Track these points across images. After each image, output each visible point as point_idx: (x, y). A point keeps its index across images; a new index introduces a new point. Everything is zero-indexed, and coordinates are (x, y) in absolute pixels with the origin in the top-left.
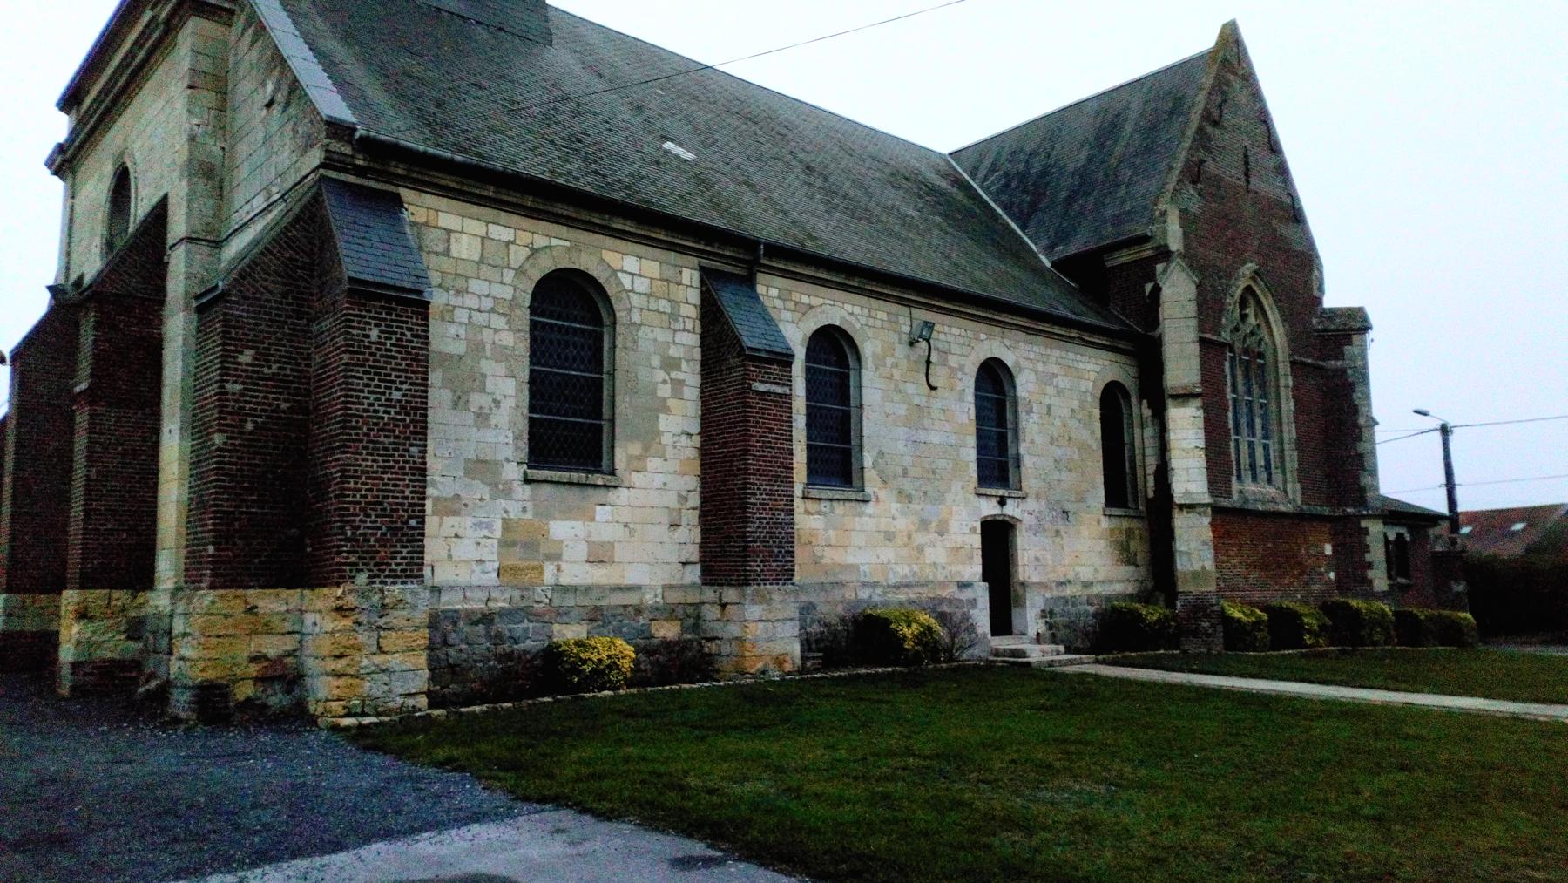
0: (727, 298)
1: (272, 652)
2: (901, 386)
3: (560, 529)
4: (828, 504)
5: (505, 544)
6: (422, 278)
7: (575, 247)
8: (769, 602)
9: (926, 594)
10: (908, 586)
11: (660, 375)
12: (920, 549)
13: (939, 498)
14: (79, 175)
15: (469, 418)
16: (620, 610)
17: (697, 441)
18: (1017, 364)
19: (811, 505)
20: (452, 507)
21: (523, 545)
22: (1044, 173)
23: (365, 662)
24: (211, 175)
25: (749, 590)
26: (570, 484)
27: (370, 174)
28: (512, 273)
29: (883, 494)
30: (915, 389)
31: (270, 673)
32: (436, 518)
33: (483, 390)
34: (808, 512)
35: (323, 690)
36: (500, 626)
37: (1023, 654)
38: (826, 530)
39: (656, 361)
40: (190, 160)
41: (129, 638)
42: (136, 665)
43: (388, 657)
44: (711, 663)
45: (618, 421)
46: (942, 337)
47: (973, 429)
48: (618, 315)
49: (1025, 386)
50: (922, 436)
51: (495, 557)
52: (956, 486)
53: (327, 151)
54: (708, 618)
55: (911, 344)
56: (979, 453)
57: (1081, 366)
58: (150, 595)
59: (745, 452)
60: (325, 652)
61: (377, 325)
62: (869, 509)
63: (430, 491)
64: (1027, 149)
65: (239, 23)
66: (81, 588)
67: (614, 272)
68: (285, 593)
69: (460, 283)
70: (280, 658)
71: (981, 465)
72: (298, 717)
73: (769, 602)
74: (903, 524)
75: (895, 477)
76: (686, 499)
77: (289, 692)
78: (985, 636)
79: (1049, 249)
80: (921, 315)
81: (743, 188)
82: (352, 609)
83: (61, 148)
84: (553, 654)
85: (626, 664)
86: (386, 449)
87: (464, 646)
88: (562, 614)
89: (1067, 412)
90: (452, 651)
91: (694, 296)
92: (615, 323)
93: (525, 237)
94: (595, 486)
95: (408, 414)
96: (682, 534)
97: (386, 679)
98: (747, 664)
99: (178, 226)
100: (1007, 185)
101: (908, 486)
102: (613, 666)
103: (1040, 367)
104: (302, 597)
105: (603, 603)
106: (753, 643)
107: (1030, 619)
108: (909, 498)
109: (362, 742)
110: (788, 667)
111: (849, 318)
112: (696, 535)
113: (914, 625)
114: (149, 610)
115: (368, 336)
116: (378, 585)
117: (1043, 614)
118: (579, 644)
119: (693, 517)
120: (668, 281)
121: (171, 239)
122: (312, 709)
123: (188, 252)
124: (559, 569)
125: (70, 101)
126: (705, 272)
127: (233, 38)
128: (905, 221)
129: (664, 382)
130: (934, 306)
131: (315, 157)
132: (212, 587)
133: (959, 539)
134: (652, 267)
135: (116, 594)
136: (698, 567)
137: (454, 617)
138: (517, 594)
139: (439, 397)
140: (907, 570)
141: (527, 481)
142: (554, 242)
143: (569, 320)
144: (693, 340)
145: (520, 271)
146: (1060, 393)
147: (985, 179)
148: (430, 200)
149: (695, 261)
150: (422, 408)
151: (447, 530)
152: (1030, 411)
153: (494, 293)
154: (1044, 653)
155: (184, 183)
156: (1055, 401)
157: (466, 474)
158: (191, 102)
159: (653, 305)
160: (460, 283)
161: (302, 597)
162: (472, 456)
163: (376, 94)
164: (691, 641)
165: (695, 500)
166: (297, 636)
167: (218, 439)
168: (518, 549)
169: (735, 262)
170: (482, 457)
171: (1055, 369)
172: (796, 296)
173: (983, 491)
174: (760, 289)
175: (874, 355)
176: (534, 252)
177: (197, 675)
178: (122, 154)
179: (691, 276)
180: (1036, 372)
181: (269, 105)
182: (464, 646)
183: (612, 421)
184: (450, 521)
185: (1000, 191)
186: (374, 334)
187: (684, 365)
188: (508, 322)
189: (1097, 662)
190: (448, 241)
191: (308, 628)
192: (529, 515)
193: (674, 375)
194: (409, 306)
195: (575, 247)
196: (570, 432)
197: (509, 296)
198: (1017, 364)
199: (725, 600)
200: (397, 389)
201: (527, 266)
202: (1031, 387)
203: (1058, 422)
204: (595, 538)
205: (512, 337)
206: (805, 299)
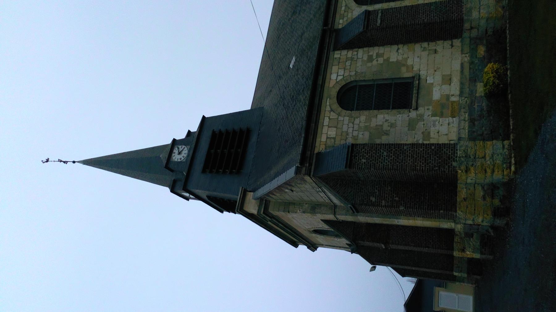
1: (482, 193)
3: (436, 95)
5: (442, 115)
11: (375, 62)
17: (400, 46)
20: (427, 135)
21: (443, 108)
24: (314, 208)
25: (465, 18)
26: (418, 93)
27: (311, 162)
28: (340, 117)
32: (431, 140)
33: (382, 126)
39: (369, 64)
40: (310, 213)
41: (472, 237)
43: (487, 154)
45: (393, 77)
51: (447, 119)
58: (456, 230)
61: (361, 160)
63: (420, 142)
67: (337, 82)
68: (459, 189)
72: (509, 186)
76: (425, 48)
77: (498, 188)
85: (496, 66)
88: (472, 93)
90: (485, 133)
91: (344, 52)
93: (327, 114)
95: (392, 150)
96: (439, 48)
99: (331, 217)
102: (497, 71)
104: (461, 183)
105: (468, 77)
112: (440, 42)
118: (485, 86)
120: (339, 62)
123: (339, 215)
124: (453, 95)
126: (335, 49)
129: (377, 61)
131: (307, 178)
132: (456, 211)
134: (335, 69)
135: (456, 240)
137: (471, 132)
139: (384, 140)
141: (417, 109)
142: (328, 104)
143: (353, 97)
144: (361, 51)
145: (339, 115)
150: (390, 145)
158: (293, 212)
159: (348, 67)
160: (344, 134)
165: (425, 44)
166: (476, 185)
167: (402, 208)
169: (330, 39)
172: (342, 12)
174: (340, 27)
176: (332, 110)
177: (489, 217)
178: (309, 231)
179: (337, 54)
181: (292, 191)
182: (484, 128)
183: (392, 79)
184: (432, 135)
186: (364, 161)
187: (370, 54)
192: (431, 107)
193: (374, 57)
194: (353, 151)
196: (399, 93)
197: (348, 118)
199: (469, 28)
200: (383, 153)
205: (362, 117)
206: (343, 8)
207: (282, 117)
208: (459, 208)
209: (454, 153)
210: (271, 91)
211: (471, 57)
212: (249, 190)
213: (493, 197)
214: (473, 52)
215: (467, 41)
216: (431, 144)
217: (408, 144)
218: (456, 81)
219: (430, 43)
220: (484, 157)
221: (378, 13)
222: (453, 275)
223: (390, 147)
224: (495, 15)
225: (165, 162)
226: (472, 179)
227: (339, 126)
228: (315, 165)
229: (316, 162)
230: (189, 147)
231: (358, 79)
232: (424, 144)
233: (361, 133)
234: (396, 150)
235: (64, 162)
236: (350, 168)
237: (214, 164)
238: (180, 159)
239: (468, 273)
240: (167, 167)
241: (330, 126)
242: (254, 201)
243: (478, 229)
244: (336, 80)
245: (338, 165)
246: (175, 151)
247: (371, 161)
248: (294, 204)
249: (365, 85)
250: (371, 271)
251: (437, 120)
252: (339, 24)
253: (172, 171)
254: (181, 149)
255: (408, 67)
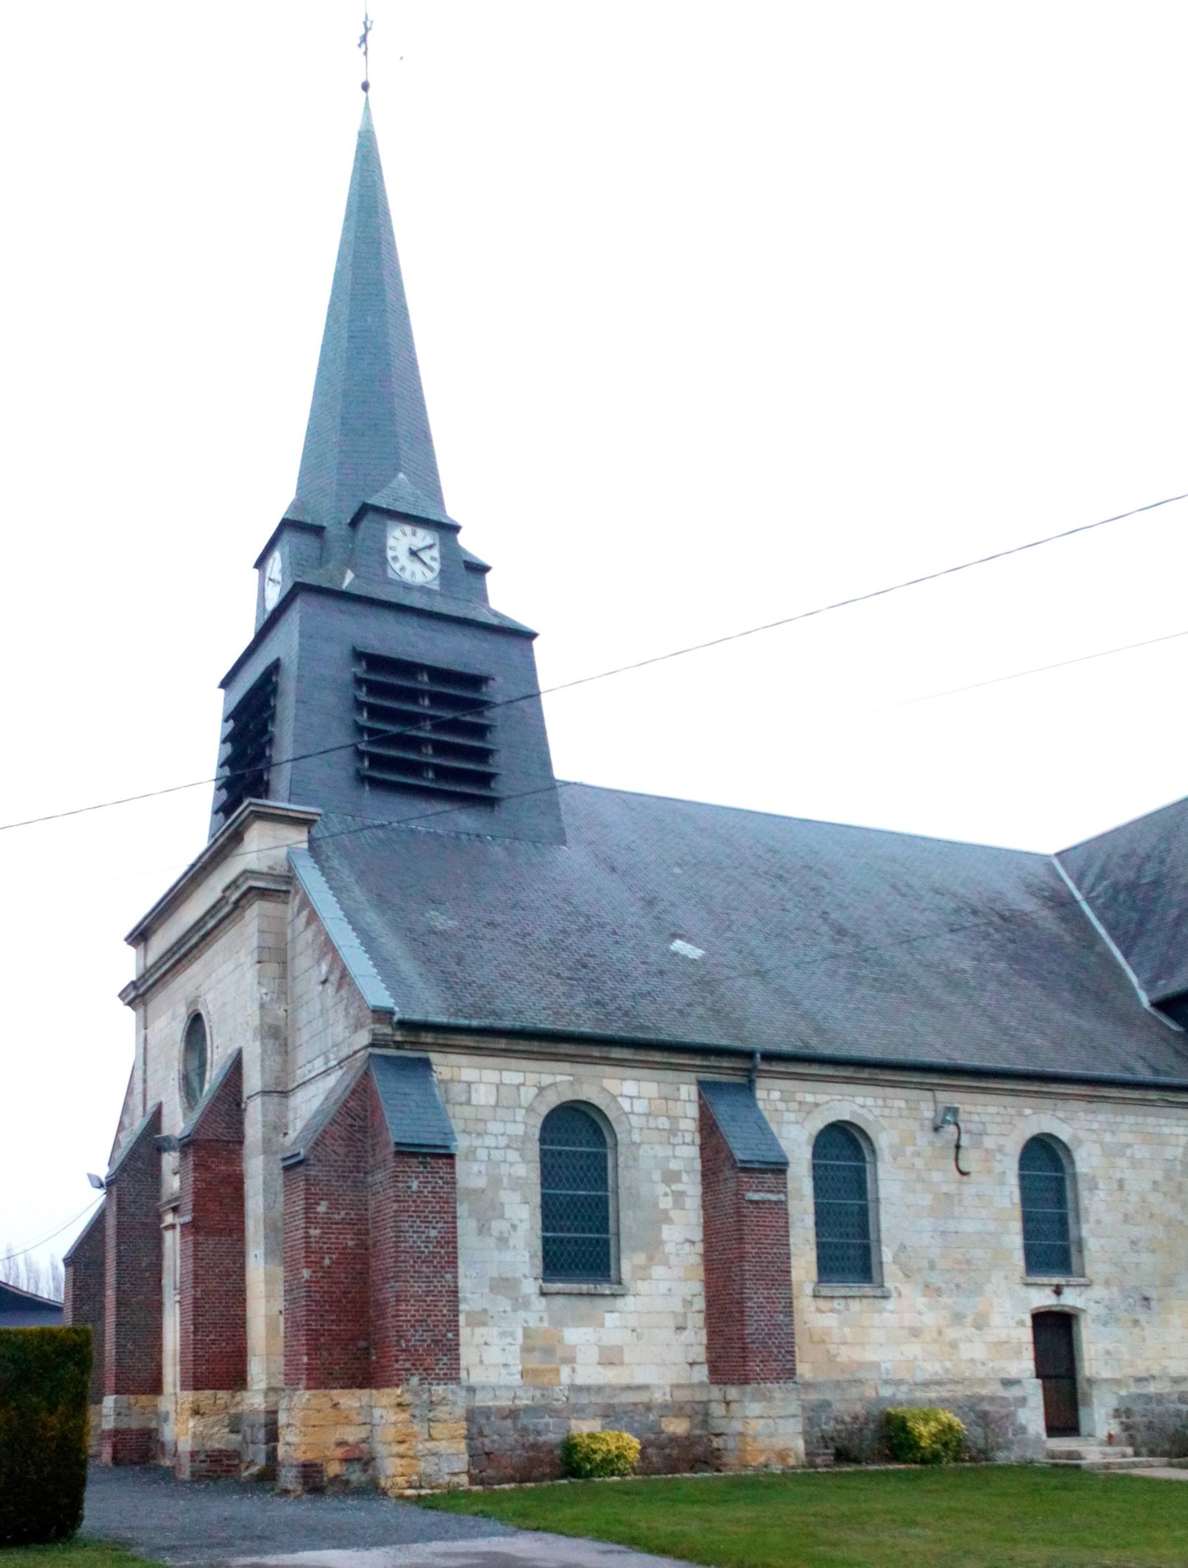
0: (721, 1110)
1: (351, 1439)
2: (925, 1175)
3: (573, 1335)
4: (842, 1301)
5: (527, 1350)
6: (449, 1134)
7: (577, 1081)
8: (770, 1399)
9: (960, 1391)
10: (939, 1383)
11: (661, 1188)
12: (954, 1345)
13: (977, 1289)
14: (151, 1008)
15: (492, 1242)
16: (631, 1408)
17: (700, 1248)
18: (1075, 1137)
19: (822, 1304)
20: (481, 1319)
21: (542, 1351)
22: (1156, 883)
23: (420, 1447)
24: (278, 1036)
25: (748, 1388)
26: (581, 1294)
27: (408, 1044)
28: (523, 1111)
29: (906, 1290)
30: (943, 1177)
31: (351, 1456)
32: (469, 1330)
33: (502, 1216)
34: (819, 1311)
35: (391, 1469)
36: (525, 1420)
37: (1078, 1456)
38: (840, 1328)
39: (657, 1176)
40: (261, 1025)
41: (232, 1432)
42: (237, 1454)
43: (437, 1443)
44: (719, 1458)
45: (622, 1237)
46: (976, 1118)
47: (1017, 1213)
48: (619, 1137)
49: (1086, 1160)
50: (952, 1225)
51: (518, 1361)
52: (997, 1277)
53: (374, 1034)
54: (715, 1415)
55: (936, 1129)
56: (1025, 1238)
57: (1166, 1130)
58: (245, 1394)
59: (742, 1258)
60: (390, 1439)
61: (417, 1178)
62: (890, 1305)
63: (462, 1307)
64: (1141, 852)
65: (295, 903)
66: (196, 1389)
67: (614, 1098)
69: (480, 1127)
70: (357, 1445)
71: (1029, 1252)
72: (372, 1490)
73: (770, 1399)
74: (930, 1319)
75: (920, 1270)
76: (691, 1303)
77: (365, 1471)
78: (1038, 1437)
79: (1149, 985)
80: (946, 1098)
81: (754, 981)
82: (408, 1405)
83: (134, 985)
84: (569, 1446)
85: (633, 1455)
86: (427, 1277)
87: (496, 1437)
88: (579, 1411)
89: (1147, 1186)
90: (486, 1441)
91: (693, 1111)
92: (616, 1145)
93: (532, 1078)
94: (603, 1295)
95: (442, 1247)
96: (688, 1336)
97: (437, 1461)
98: (749, 1458)
99: (253, 1080)
100: (1114, 898)
101: (936, 1279)
103: (1108, 1138)
104: (371, 1396)
105: (615, 1401)
106: (755, 1439)
107: (1099, 1417)
108: (939, 1292)
109: (421, 1504)
110: (792, 1461)
111: (861, 1111)
112: (703, 1337)
113: (933, 1424)
114: (244, 1407)
115: (409, 1187)
116: (426, 1386)
117: (1117, 1413)
118: (592, 1436)
119: (699, 1320)
120: (666, 1099)
121: (246, 1092)
122: (383, 1483)
123: (263, 1104)
124: (573, 1370)
125: (140, 936)
126: (702, 1084)
127: (289, 917)
128: (952, 980)
129: (666, 1195)
130: (953, 1086)
131: (364, 1038)
132: (308, 1388)
133: (1003, 1334)
135: (221, 1394)
136: (706, 1367)
137: (487, 1412)
138: (538, 1393)
139: (466, 1226)
140: (937, 1367)
141: (543, 1294)
142: (559, 1078)
143: (576, 1145)
144: (694, 1152)
145: (530, 1109)
146: (1135, 1164)
147: (1092, 890)
148: (453, 1059)
149: (692, 1076)
151: (478, 1340)
152: (1094, 1188)
153: (508, 1132)
154: (1105, 1455)
155: (258, 1044)
156: (1128, 1174)
157: (492, 1289)
158: (261, 975)
159: (652, 1124)
160: (480, 1127)
161: (371, 1396)
162: (495, 1275)
163: (408, 968)
164: (700, 1437)
165: (700, 1304)
166: (368, 1427)
167: (306, 1273)
168: (537, 1354)
169: (730, 1070)
170: (504, 1276)
171: (1129, 1138)
173: (1031, 1280)
174: (760, 1094)
175: (891, 1146)
176: (541, 1089)
177: (300, 1456)
178: (195, 1001)
179: (688, 1091)
180: (1102, 1144)
181: (324, 982)
182: (496, 1437)
183: (618, 1235)
184: (480, 1331)
185: (1106, 907)
186: (415, 1185)
187: (685, 1177)
188: (522, 1156)
189: (1171, 1465)
190: (469, 1092)
191: (376, 1421)
192: (546, 1324)
193: (675, 1187)
194: (438, 1156)
195: (577, 1081)
196: (580, 1245)
197: (521, 1133)
198: (1075, 1137)
199: (729, 1398)
200: (434, 1228)
201: (536, 1105)
202: (1095, 1161)
203: (1134, 1198)
204: (605, 1342)
206: (810, 1098)
207: (528, 929)
208: (314, 1395)
209: (439, 1379)
210: (613, 869)
211: (665, 1406)
212: (313, 831)
213: (346, 1460)
214: (676, 1410)
215: (701, 1396)
216: (457, 1331)
217: (456, 1282)
218: (609, 1376)
219: (702, 1316)
220: (431, 1438)
221: (780, 1192)
222: (104, 1394)
223: (448, 1242)
224: (749, 1448)
225: (379, 500)
226: (382, 1417)
227: (501, 1113)
228: (400, 1058)
229: (406, 1058)
230: (435, 586)
231: (621, 1149)
232: (457, 1316)
233: (483, 1168)
234: (442, 1257)
235: (364, 39)
236: (398, 1154)
237: (388, 708)
238: (395, 559)
239: (116, 1432)
240: (365, 510)
241: (502, 1088)
242: (282, 852)
243: (253, 1443)
244: (622, 1096)
245: (400, 1124)
246: (421, 532)
247: (415, 1201)
248: (283, 976)
249: (605, 1169)
250: (90, 1176)
251: (515, 1339)
252: (769, 1091)
253: (354, 523)
254: (425, 556)
255: (644, 1268)
